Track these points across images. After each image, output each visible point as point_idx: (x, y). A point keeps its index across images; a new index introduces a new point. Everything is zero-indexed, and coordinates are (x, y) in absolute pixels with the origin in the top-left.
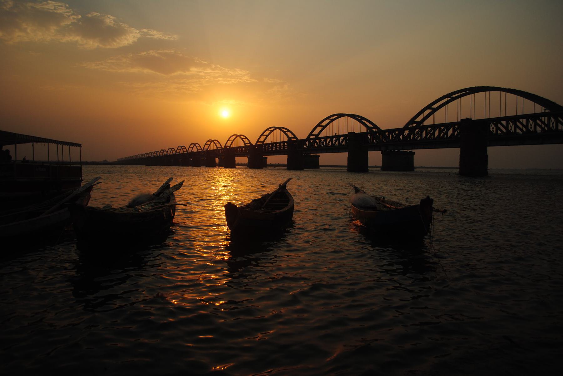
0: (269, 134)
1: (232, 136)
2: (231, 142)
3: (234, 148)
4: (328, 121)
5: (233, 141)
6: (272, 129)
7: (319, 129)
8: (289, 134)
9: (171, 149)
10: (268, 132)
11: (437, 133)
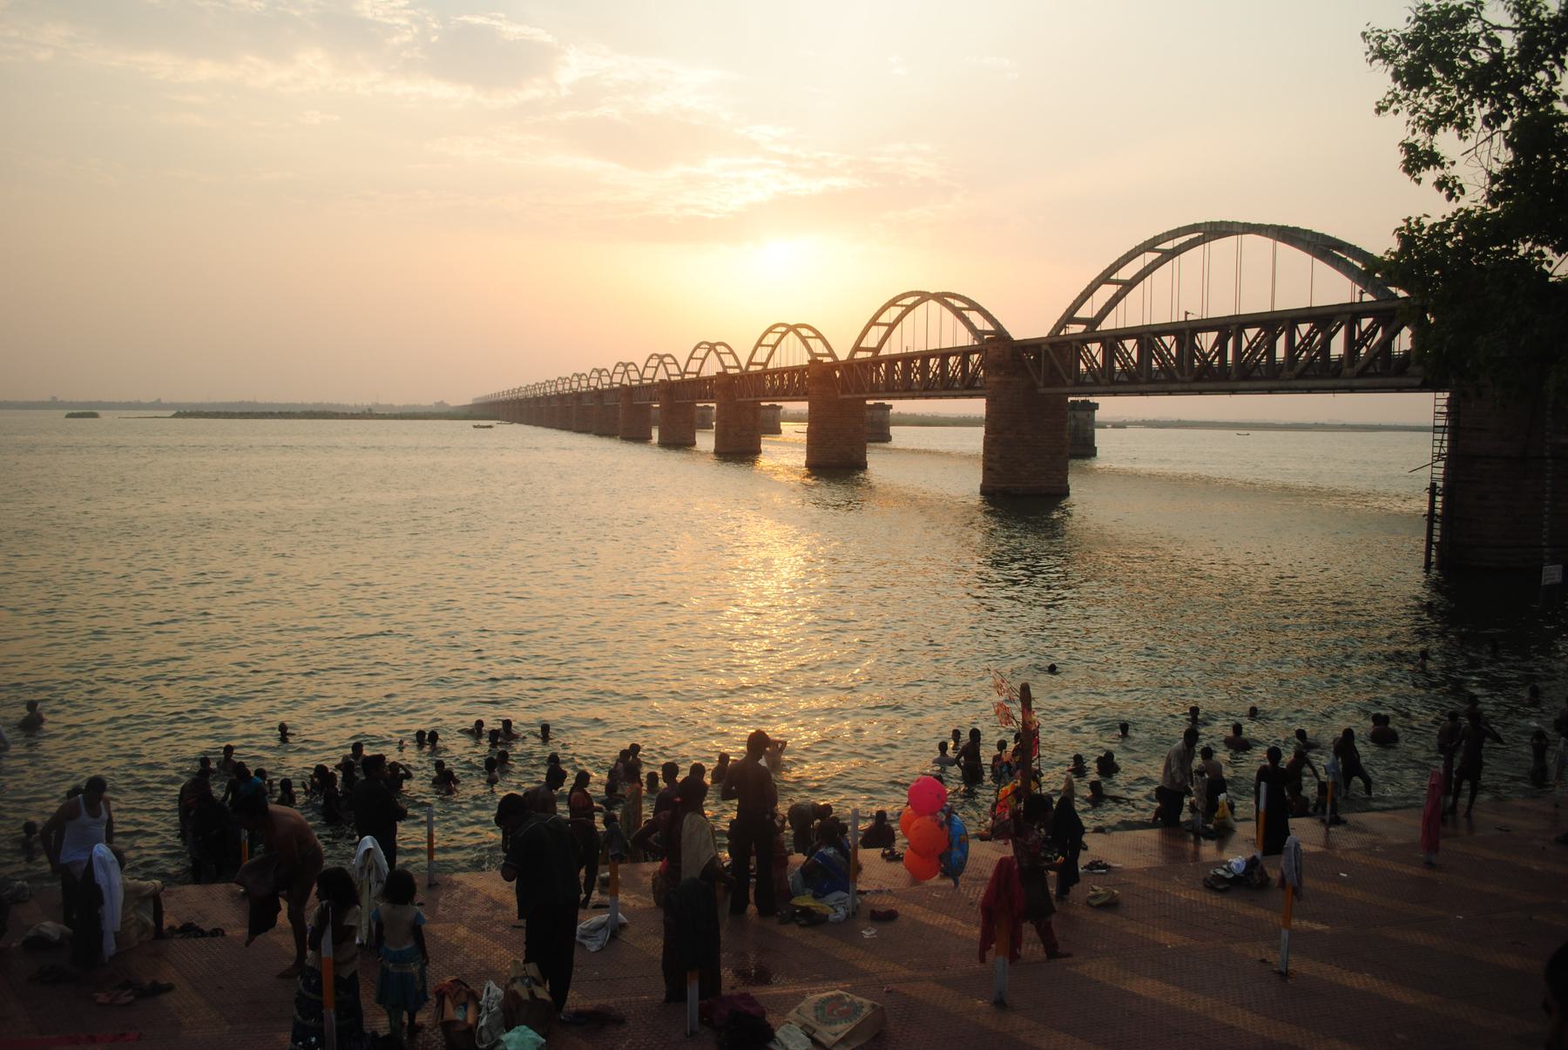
0: (900, 319)
1: (770, 330)
2: (766, 351)
3: (780, 372)
4: (1150, 257)
5: (774, 347)
6: (909, 301)
7: (1106, 292)
8: (974, 317)
9: (626, 366)
10: (894, 312)
11: (1338, 346)
